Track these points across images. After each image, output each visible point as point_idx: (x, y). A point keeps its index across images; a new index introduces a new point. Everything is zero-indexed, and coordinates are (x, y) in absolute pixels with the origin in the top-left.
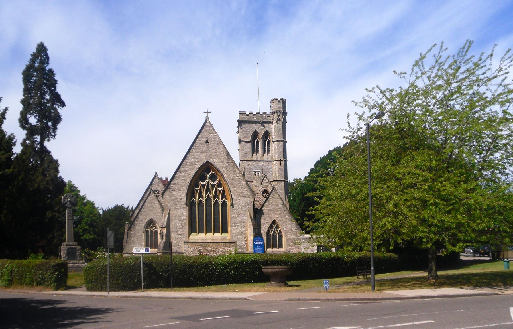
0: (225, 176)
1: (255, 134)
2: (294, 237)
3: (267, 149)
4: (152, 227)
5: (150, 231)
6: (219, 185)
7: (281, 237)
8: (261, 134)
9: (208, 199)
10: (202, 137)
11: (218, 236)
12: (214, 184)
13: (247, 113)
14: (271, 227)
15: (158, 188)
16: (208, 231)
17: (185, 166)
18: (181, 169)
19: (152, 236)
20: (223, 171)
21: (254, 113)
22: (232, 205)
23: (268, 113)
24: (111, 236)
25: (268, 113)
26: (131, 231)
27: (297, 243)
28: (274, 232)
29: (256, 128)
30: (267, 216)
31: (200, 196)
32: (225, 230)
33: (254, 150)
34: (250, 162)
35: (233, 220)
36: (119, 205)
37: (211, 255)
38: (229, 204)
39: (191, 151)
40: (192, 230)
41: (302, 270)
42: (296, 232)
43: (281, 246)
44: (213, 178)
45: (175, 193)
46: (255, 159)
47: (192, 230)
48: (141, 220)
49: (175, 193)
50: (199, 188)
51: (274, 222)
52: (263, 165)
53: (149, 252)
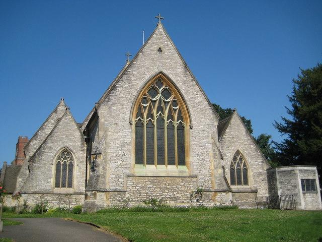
0: (183, 92)
2: (261, 171)
4: (65, 158)
5: (62, 163)
7: (246, 170)
9: (161, 120)
11: (173, 170)
14: (235, 159)
16: (161, 162)
19: (65, 170)
20: (180, 85)
26: (34, 161)
28: (239, 165)
30: (229, 146)
31: (150, 115)
35: (194, 148)
42: (262, 165)
43: (246, 183)
47: (139, 160)
48: (51, 148)
50: (148, 104)
51: (238, 153)
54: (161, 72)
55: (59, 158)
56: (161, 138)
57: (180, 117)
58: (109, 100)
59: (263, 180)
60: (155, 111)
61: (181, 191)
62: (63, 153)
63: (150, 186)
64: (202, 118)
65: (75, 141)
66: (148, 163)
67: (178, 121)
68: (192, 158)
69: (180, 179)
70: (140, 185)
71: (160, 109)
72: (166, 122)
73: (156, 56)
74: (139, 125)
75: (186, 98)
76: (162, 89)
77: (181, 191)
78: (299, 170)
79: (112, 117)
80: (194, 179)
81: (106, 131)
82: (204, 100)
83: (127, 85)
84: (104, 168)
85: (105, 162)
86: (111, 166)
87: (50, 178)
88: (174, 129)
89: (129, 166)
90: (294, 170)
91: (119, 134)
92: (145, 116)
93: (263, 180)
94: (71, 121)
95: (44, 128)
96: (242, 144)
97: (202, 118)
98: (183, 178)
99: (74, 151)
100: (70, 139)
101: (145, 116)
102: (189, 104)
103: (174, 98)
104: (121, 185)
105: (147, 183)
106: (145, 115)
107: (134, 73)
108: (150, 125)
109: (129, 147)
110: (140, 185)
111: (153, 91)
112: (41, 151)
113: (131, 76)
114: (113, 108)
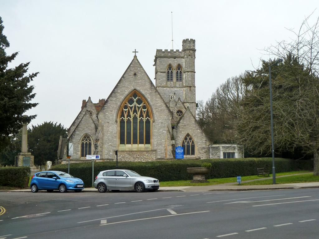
0: (149, 100)
1: (170, 67)
2: (204, 146)
3: (179, 78)
4: (86, 140)
5: (85, 143)
6: (144, 107)
8: (175, 65)
9: (135, 118)
10: (131, 70)
12: (131, 106)
13: (163, 50)
14: (186, 139)
15: (91, 109)
16: (135, 142)
17: (116, 93)
18: (113, 95)
19: (86, 147)
20: (148, 96)
21: (169, 50)
22: (154, 122)
23: (180, 51)
24: (72, 146)
25: (180, 51)
27: (203, 151)
28: (188, 143)
29: (170, 62)
30: (182, 131)
32: (148, 142)
33: (169, 78)
34: (165, 88)
36: (48, 122)
37: (136, 161)
38: (151, 122)
39: (122, 81)
40: (122, 142)
41: (217, 171)
42: (206, 143)
43: (193, 153)
44: (139, 102)
45: (107, 113)
46: (169, 86)
47: (122, 142)
48: (78, 135)
49: (107, 113)
50: (127, 109)
51: (188, 135)
52: (176, 90)
53: (99, 159)
54: (135, 89)
55: (83, 140)
56: (135, 129)
57: (148, 115)
58: (104, 109)
59: (205, 152)
60: (131, 113)
61: (146, 159)
62: (85, 137)
63: (127, 156)
64: (161, 115)
65: (92, 130)
66: (127, 143)
67: (146, 117)
68: (153, 140)
69: (145, 152)
70: (121, 156)
71: (135, 111)
72: (138, 119)
73: (132, 79)
74: (122, 122)
75: (151, 104)
76: (136, 99)
77: (146, 159)
78: (223, 147)
79: (106, 119)
80: (154, 152)
81: (103, 127)
82: (163, 104)
83: (114, 99)
84: (101, 147)
85: (102, 144)
86: (106, 146)
87: (79, 152)
88: (144, 123)
89: (115, 146)
90: (219, 147)
91: (110, 128)
92: (126, 116)
93: (205, 152)
94: (89, 118)
95: (79, 118)
96: (191, 129)
97: (161, 115)
98: (148, 152)
99: (91, 136)
100: (89, 129)
101: (126, 116)
102: (153, 107)
103: (144, 104)
104: (111, 156)
105: (126, 154)
106: (126, 116)
107: (119, 91)
108: (129, 121)
109: (116, 135)
110: (121, 156)
111: (131, 102)
112: (72, 137)
113: (117, 93)
114: (106, 113)
